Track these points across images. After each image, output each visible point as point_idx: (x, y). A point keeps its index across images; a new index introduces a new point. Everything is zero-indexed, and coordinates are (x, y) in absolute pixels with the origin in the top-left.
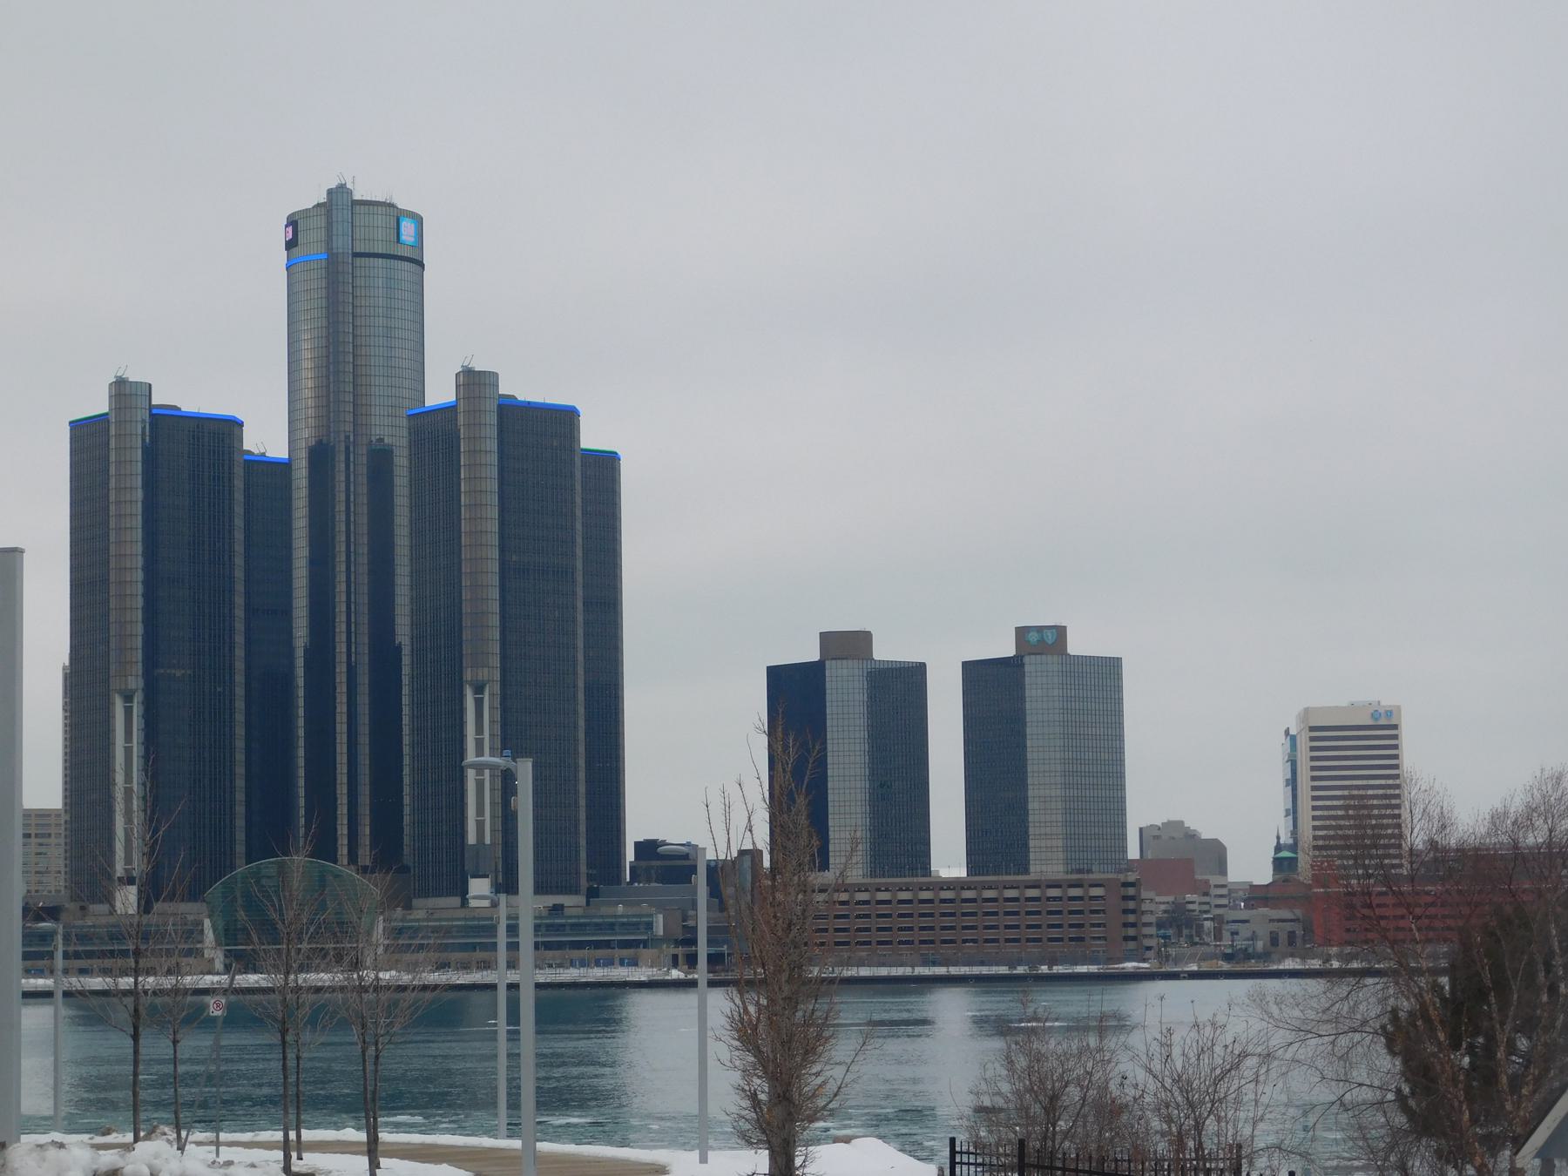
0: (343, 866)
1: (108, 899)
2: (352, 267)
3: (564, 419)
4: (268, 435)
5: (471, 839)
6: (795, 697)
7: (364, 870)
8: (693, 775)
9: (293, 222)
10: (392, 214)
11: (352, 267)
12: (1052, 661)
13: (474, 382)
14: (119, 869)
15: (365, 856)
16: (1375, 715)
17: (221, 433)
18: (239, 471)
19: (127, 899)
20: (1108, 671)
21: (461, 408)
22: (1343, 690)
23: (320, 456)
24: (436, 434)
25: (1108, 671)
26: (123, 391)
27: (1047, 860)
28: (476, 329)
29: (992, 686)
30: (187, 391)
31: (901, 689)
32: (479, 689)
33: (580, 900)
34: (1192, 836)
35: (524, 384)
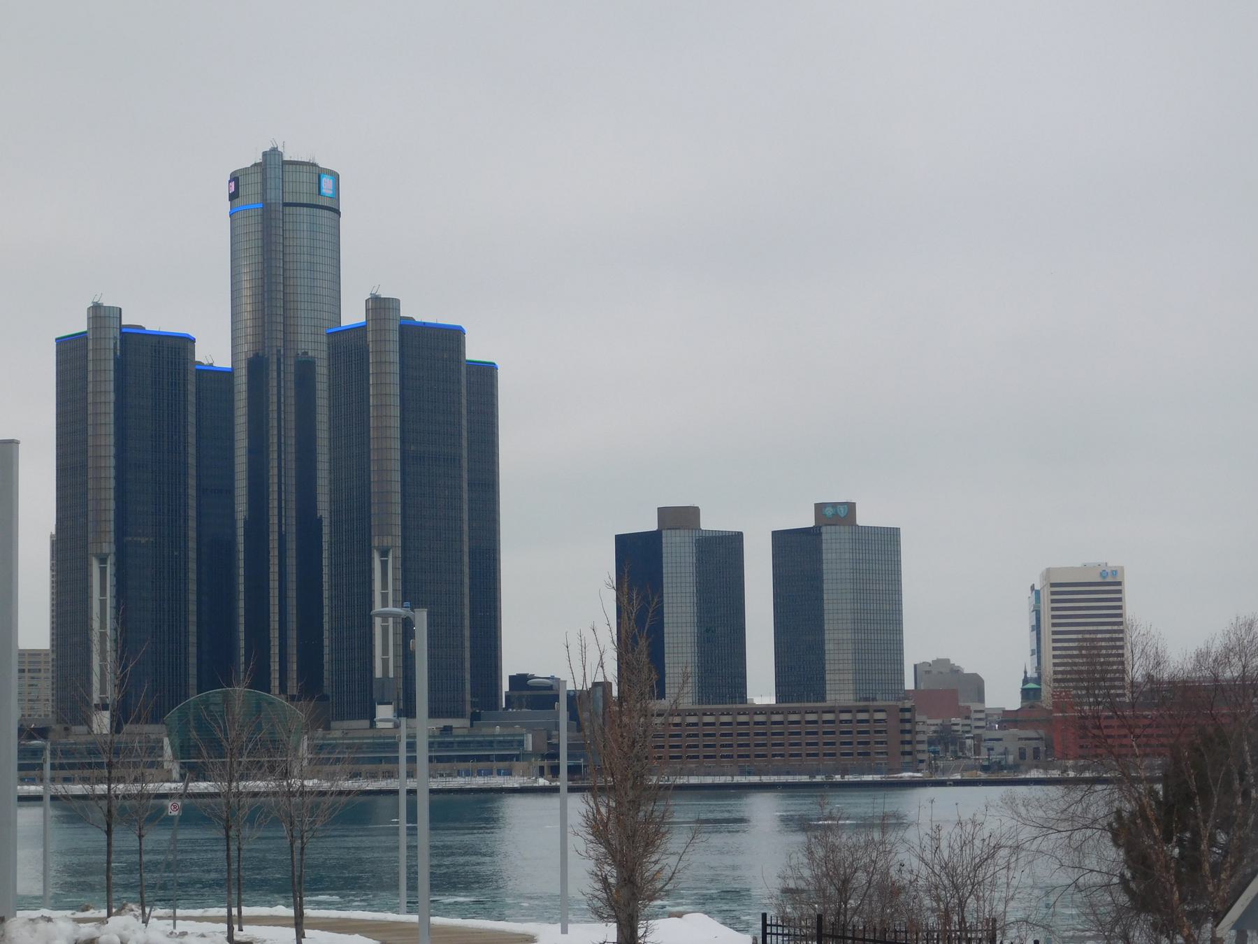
0: (275, 695)
1: (87, 721)
2: (282, 214)
3: (453, 337)
4: (215, 349)
5: (378, 673)
6: (638, 559)
7: (292, 698)
8: (556, 622)
9: (235, 178)
10: (315, 171)
11: (282, 214)
12: (844, 531)
13: (380, 307)
14: (96, 698)
15: (293, 687)
16: (1103, 574)
17: (178, 347)
18: (192, 378)
19: (102, 722)
20: (889, 539)
21: (370, 328)
22: (1078, 554)
23: (257, 366)
24: (350, 348)
25: (889, 539)
26: (99, 314)
27: (840, 690)
28: (382, 264)
29: (796, 551)
30: (150, 314)
31: (723, 553)
32: (384, 553)
33: (465, 722)
34: (956, 671)
35: (421, 308)
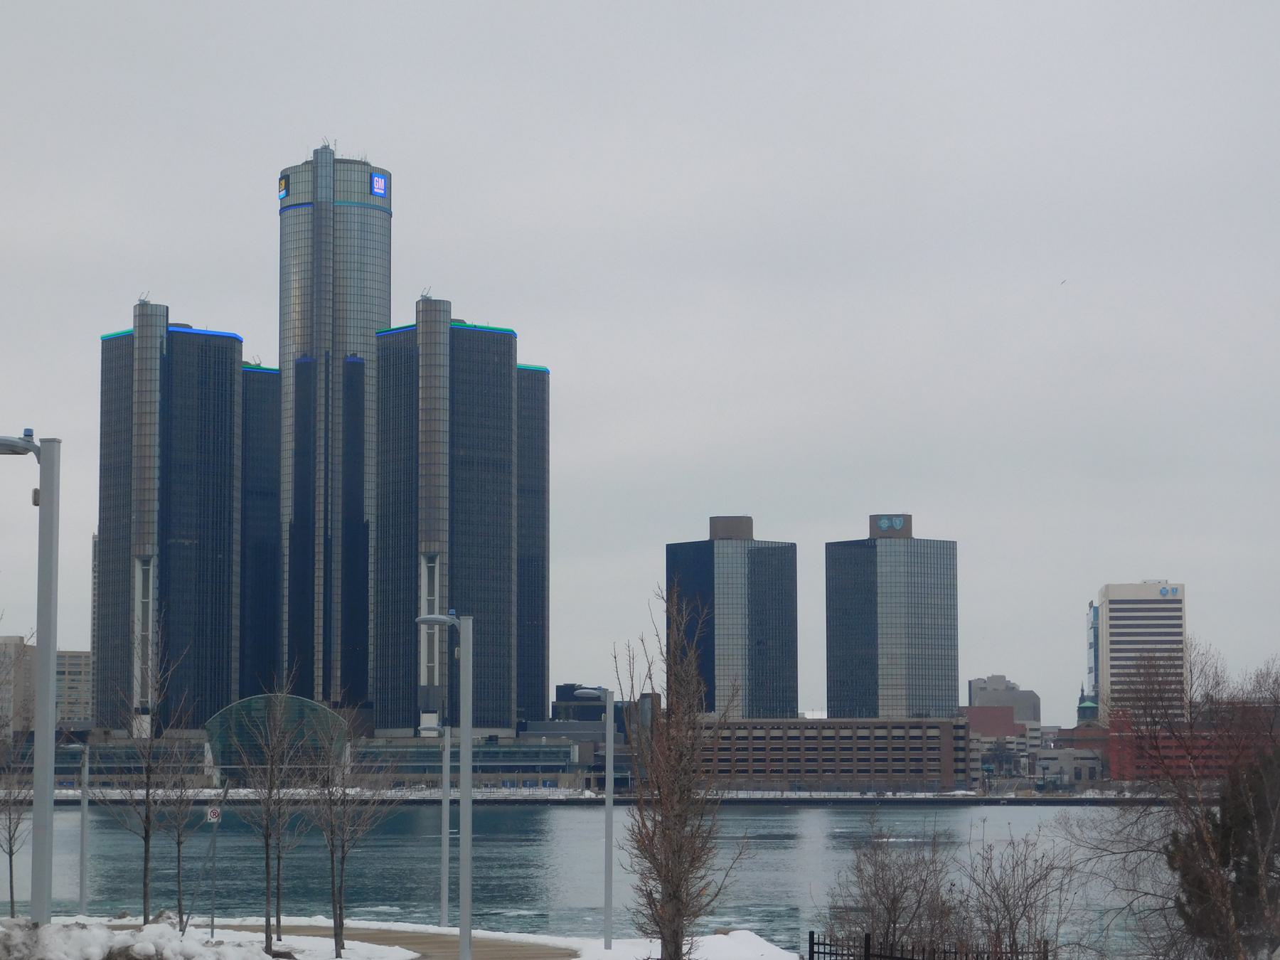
0: (318, 701)
1: (127, 725)
2: (332, 213)
3: (504, 341)
4: (263, 349)
5: (423, 681)
6: (689, 570)
8: (606, 632)
11: (332, 213)
13: (431, 309)
14: (136, 702)
16: (1164, 591)
19: (143, 726)
20: (944, 553)
21: (420, 330)
22: (1138, 571)
23: (305, 368)
24: (400, 350)
25: (944, 553)
26: (146, 313)
27: (893, 706)
28: (434, 265)
29: (849, 562)
30: (197, 313)
31: (776, 565)
34: (1011, 688)
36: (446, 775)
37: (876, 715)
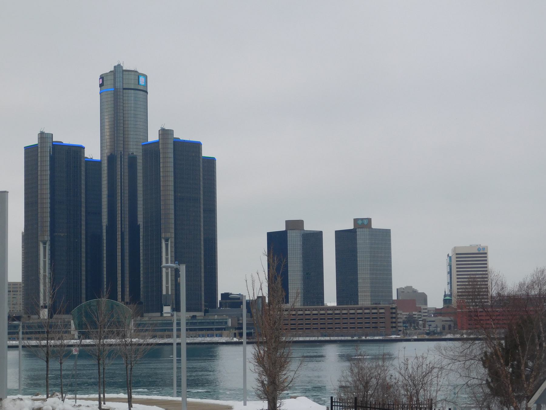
0: (119, 302)
1: (38, 313)
2: (123, 93)
3: (196, 146)
4: (93, 152)
5: (164, 292)
6: (277, 243)
7: (127, 303)
8: (241, 270)
9: (102, 77)
10: (137, 74)
11: (123, 93)
12: (366, 230)
13: (165, 133)
14: (42, 303)
15: (127, 298)
16: (479, 249)
17: (77, 151)
19: (44, 314)
20: (386, 234)
21: (161, 142)
22: (468, 241)
23: (111, 159)
24: (152, 151)
25: (386, 234)
26: (43, 136)
27: (365, 300)
28: (166, 115)
29: (345, 239)
30: (65, 136)
31: (314, 240)
32: (167, 240)
33: (202, 314)
34: (415, 291)
35: (183, 134)
36: (175, 333)
37: (357, 304)
